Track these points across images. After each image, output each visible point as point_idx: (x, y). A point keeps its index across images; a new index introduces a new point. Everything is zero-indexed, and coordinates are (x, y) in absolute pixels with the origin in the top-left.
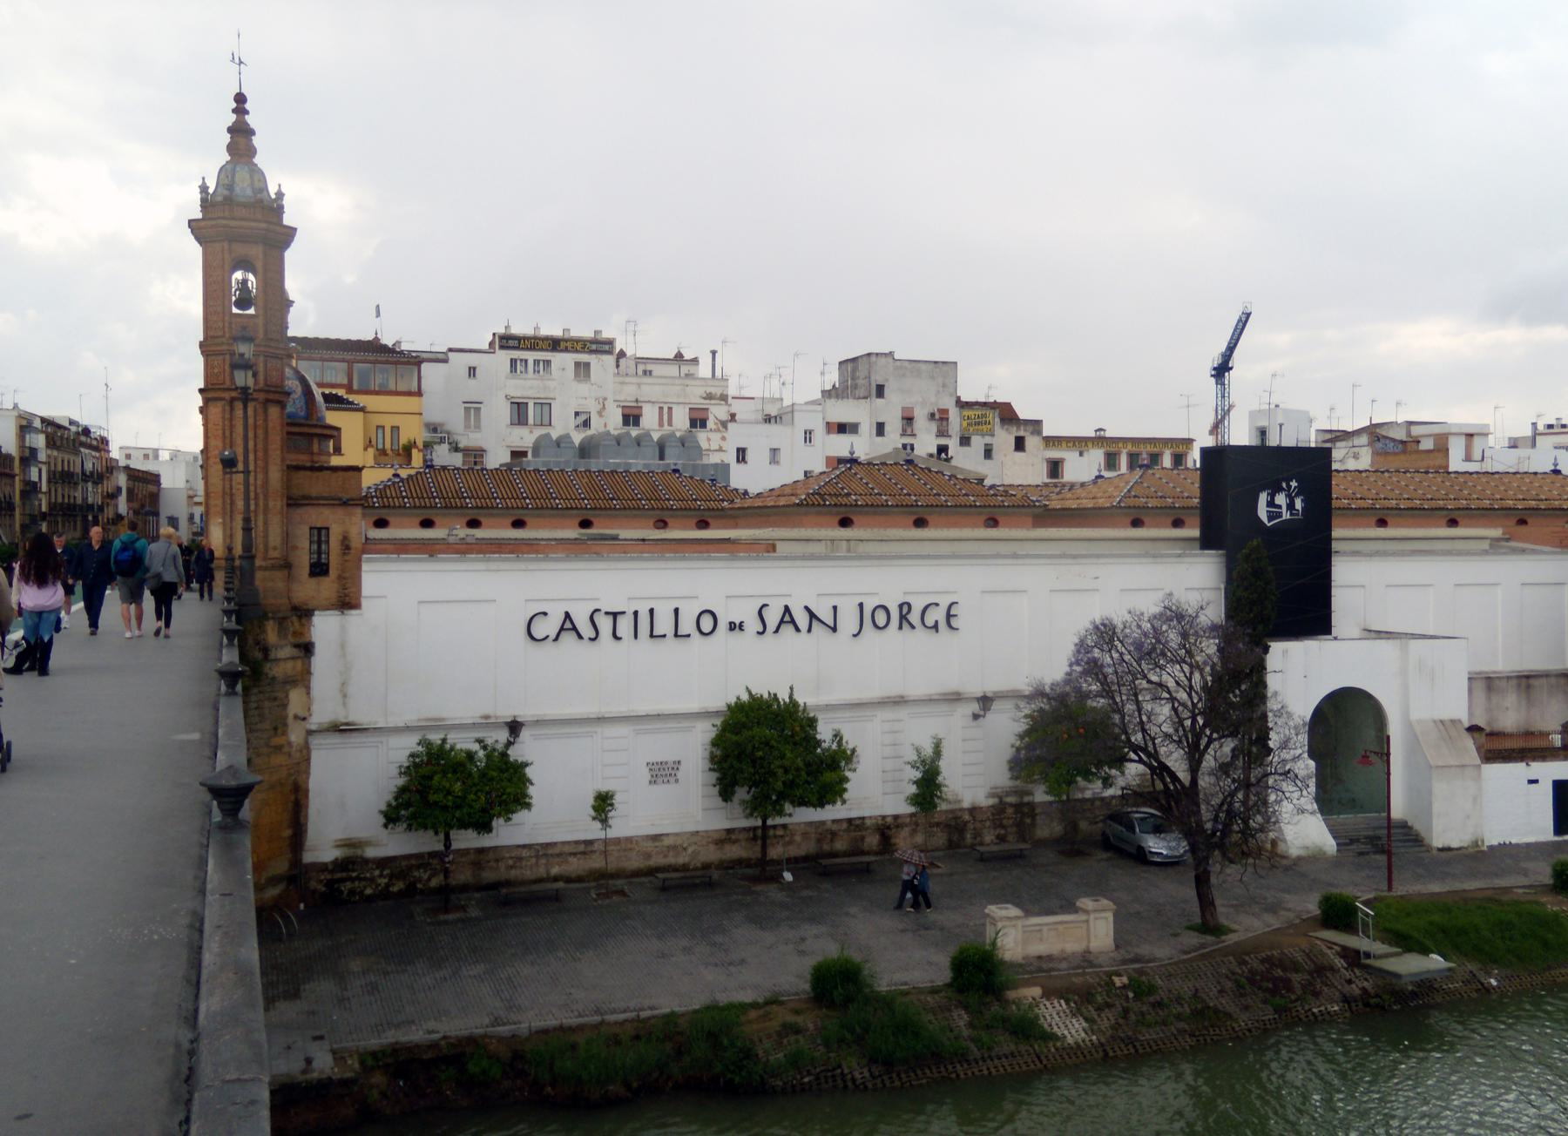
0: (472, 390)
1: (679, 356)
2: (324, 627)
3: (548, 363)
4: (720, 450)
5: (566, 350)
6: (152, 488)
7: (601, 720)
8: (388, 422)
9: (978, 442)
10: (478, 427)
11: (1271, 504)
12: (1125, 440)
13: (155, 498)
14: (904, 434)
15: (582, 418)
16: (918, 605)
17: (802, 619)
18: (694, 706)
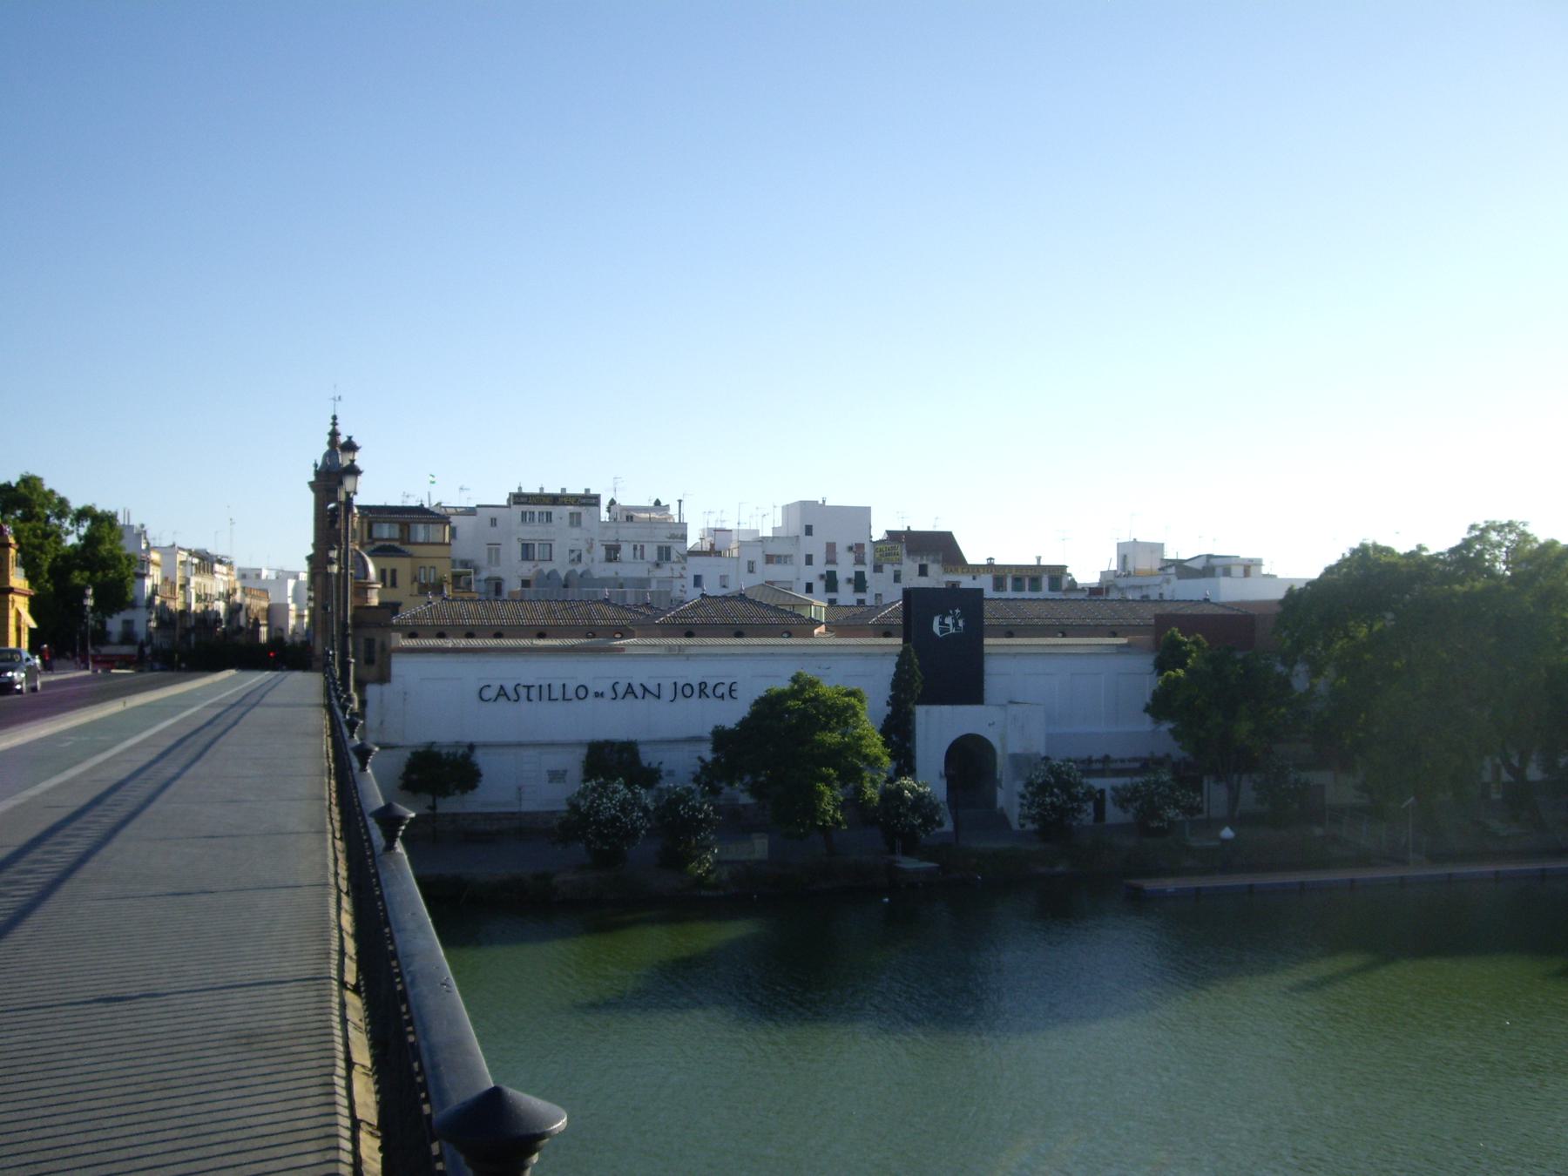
1: (658, 503)
3: (549, 514)
4: (681, 577)
5: (564, 504)
8: (428, 563)
9: (889, 570)
10: (498, 563)
14: (828, 562)
15: (574, 555)
16: (711, 683)
17: (639, 691)
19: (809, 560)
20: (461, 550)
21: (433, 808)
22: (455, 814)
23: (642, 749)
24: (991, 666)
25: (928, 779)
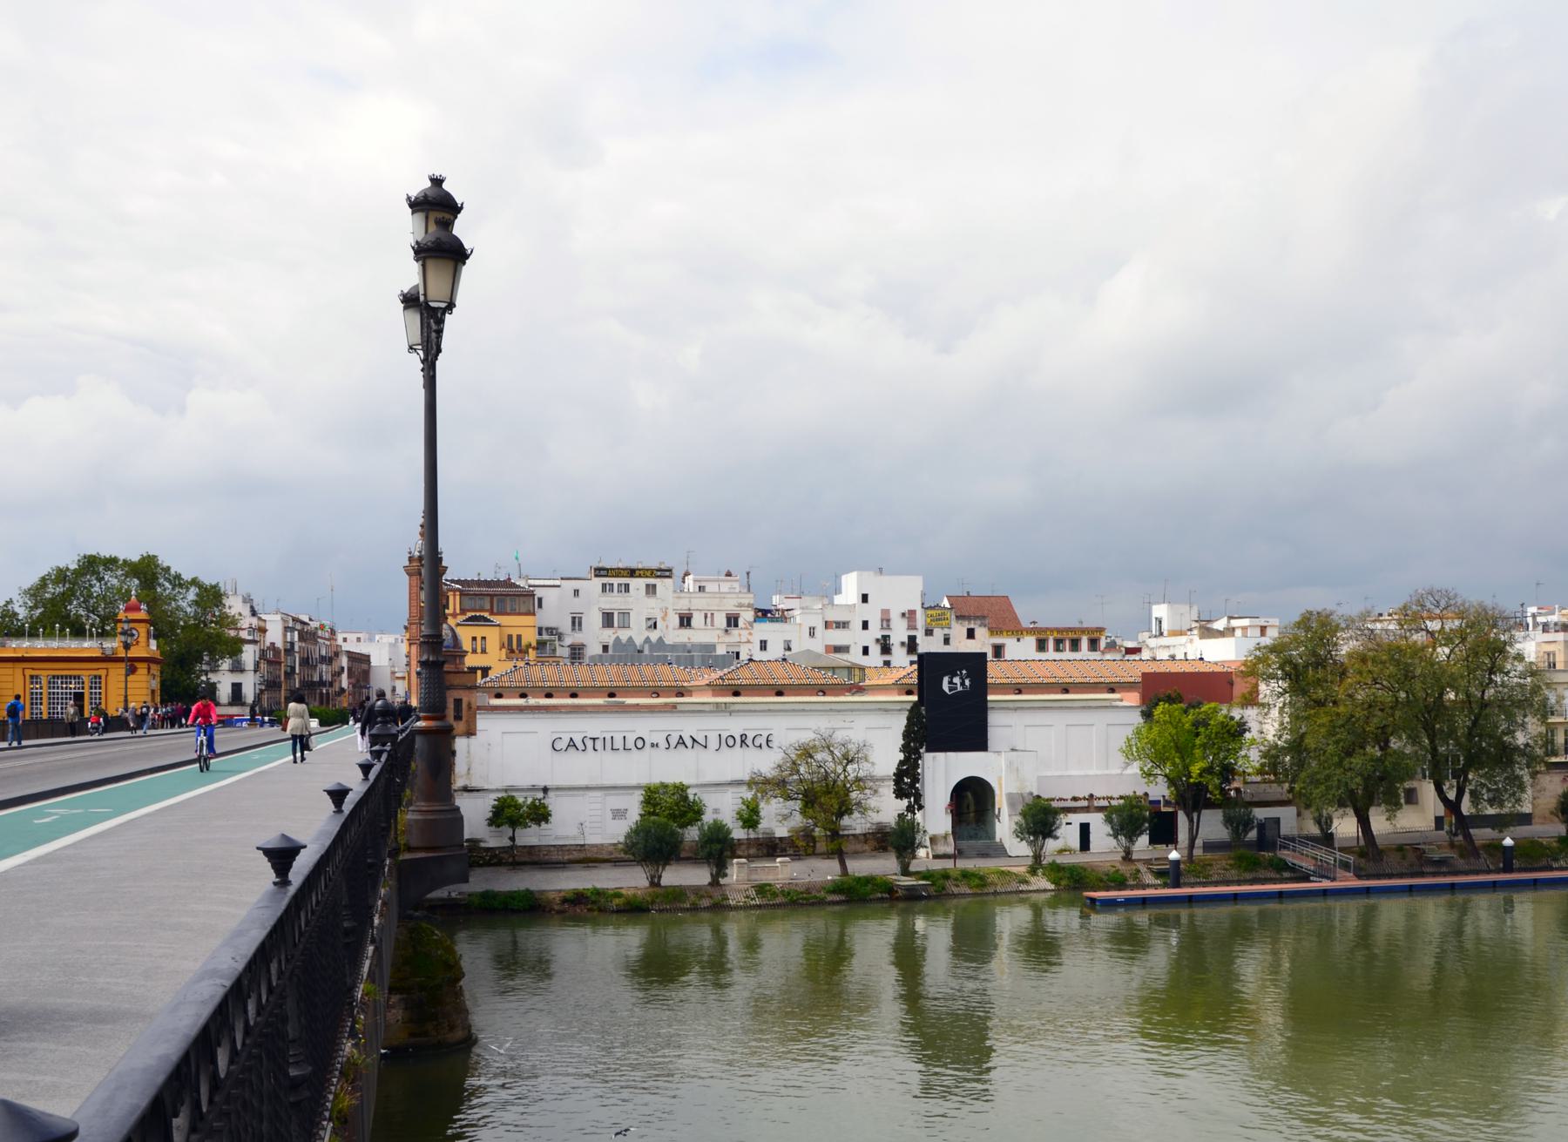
0: (576, 605)
2: (460, 744)
3: (627, 587)
6: (364, 666)
7: (587, 788)
9: (939, 634)
11: (951, 682)
12: (1052, 630)
13: (366, 674)
16: (750, 735)
17: (689, 742)
18: (634, 782)
19: (865, 625)
20: (547, 617)
21: (512, 839)
22: (532, 847)
23: (690, 792)
24: (994, 719)
25: (936, 819)
